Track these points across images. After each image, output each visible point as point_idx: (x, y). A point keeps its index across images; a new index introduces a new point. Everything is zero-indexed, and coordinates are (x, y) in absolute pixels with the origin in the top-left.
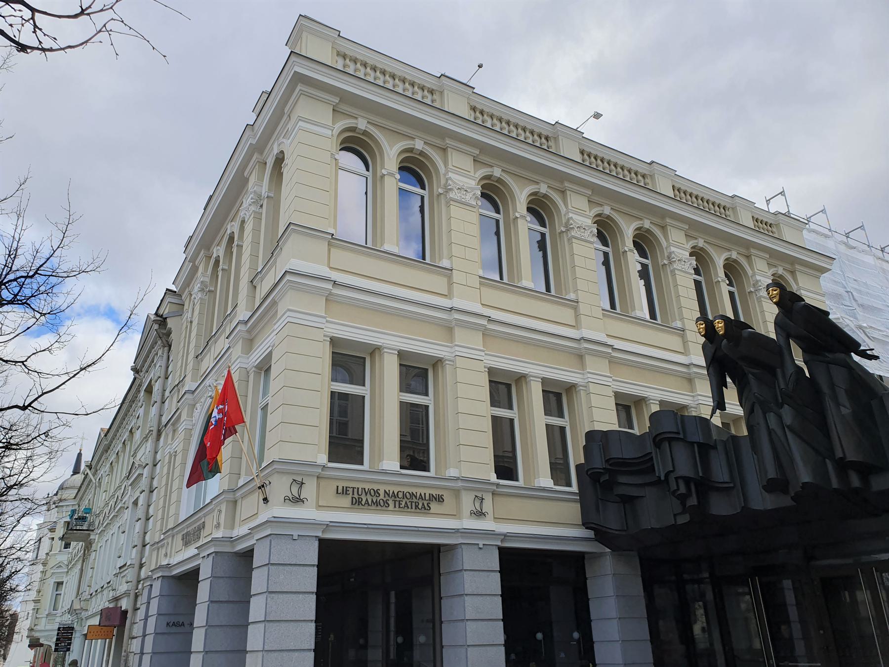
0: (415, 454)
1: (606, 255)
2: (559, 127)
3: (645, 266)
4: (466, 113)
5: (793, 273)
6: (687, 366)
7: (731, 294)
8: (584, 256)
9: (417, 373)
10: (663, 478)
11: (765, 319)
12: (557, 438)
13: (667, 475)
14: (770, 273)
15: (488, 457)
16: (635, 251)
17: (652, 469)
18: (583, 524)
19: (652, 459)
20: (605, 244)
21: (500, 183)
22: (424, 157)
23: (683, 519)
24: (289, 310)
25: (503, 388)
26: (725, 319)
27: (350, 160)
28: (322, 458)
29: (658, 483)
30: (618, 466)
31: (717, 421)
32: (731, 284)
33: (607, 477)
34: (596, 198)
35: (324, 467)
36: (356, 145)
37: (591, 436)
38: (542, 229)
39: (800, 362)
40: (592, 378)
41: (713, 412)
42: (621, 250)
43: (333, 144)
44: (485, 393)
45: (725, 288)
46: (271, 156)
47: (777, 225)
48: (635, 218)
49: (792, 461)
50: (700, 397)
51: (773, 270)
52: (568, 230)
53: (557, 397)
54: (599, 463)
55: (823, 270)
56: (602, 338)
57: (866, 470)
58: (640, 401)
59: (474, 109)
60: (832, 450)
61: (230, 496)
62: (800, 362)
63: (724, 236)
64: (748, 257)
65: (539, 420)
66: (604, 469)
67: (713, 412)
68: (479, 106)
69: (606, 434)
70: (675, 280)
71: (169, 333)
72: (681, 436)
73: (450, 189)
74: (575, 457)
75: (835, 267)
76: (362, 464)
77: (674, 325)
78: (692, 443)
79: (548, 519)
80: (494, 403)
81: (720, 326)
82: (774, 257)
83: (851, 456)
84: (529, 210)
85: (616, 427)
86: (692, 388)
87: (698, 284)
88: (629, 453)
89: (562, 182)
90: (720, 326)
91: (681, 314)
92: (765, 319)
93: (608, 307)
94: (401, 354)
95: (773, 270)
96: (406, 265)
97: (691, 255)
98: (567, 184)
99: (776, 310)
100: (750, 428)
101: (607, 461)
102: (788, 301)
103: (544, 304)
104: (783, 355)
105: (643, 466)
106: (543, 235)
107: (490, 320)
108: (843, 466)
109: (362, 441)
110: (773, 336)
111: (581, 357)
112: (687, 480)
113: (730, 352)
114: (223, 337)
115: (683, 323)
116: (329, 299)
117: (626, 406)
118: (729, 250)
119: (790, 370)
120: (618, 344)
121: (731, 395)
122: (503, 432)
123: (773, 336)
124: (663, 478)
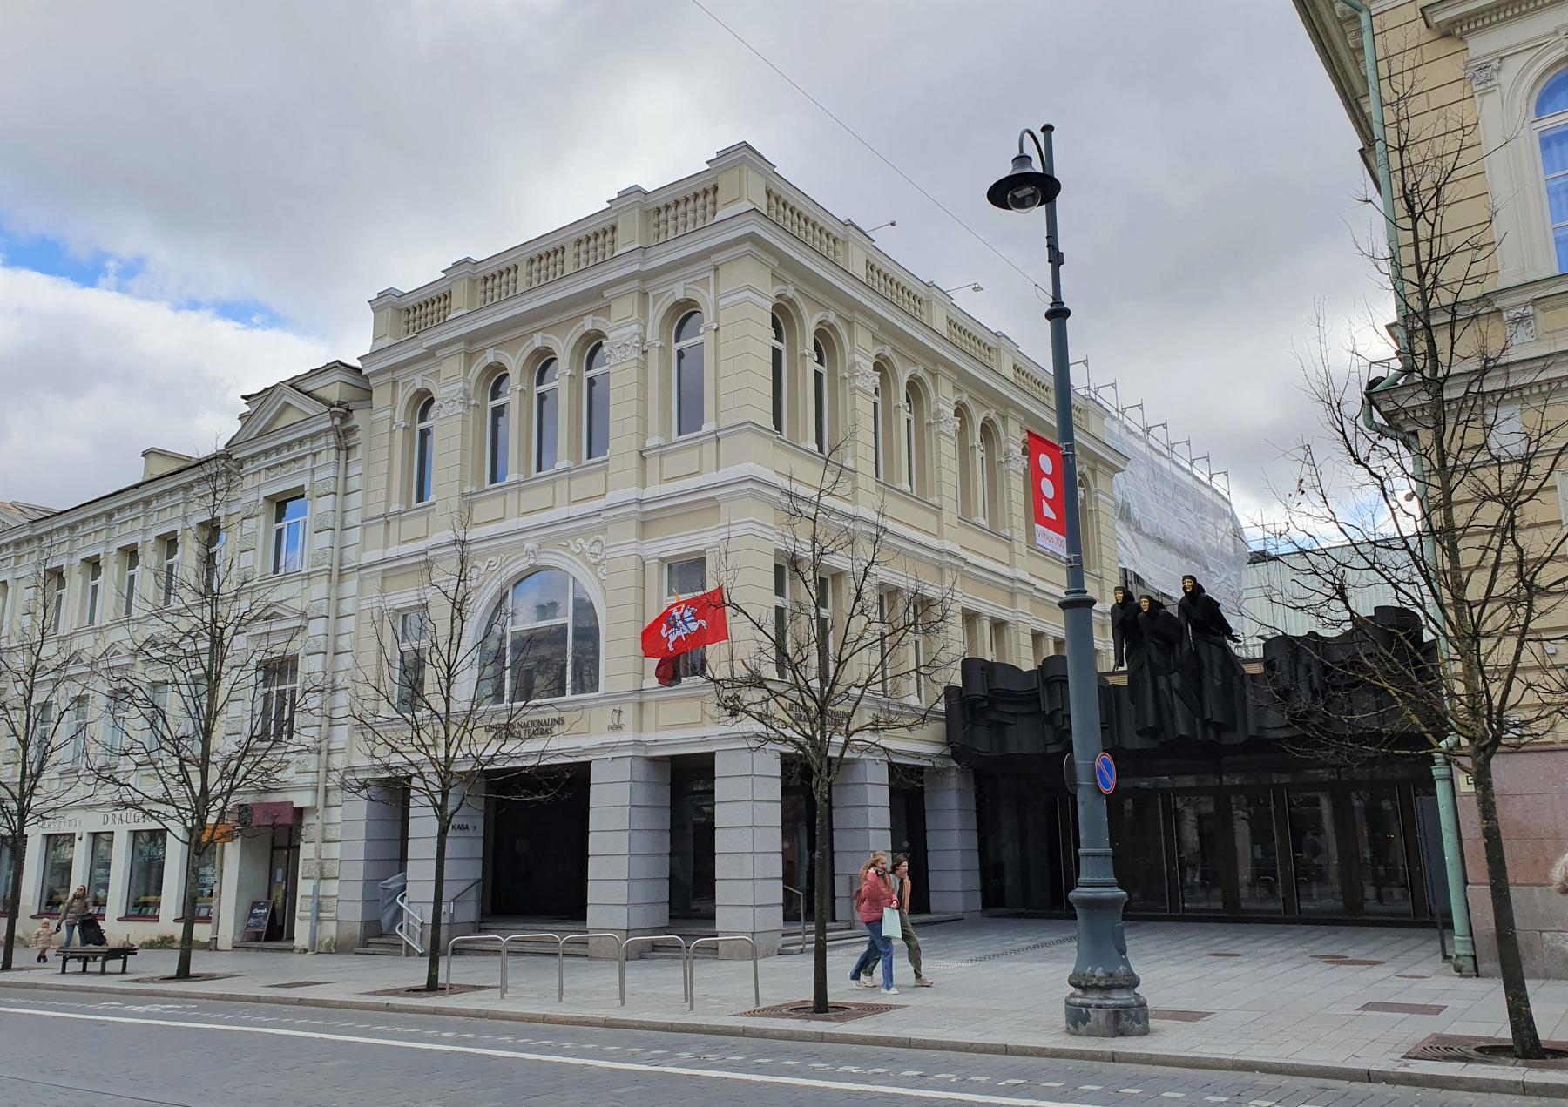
2: (935, 292)
4: (861, 271)
5: (1093, 471)
6: (1012, 580)
7: (818, 375)
8: (858, 407)
14: (772, 294)
30: (997, 697)
34: (881, 335)
40: (1022, 617)
42: (799, 352)
45: (811, 365)
47: (929, 303)
49: (1172, 715)
51: (779, 288)
52: (853, 377)
54: (979, 690)
56: (956, 549)
57: (1219, 728)
60: (1203, 712)
61: (637, 697)
64: (934, 375)
68: (878, 266)
70: (1009, 482)
71: (351, 431)
77: (975, 520)
79: (919, 744)
83: (1216, 719)
86: (1013, 605)
87: (776, 353)
89: (935, 364)
91: (1011, 521)
95: (779, 288)
98: (940, 368)
103: (1039, 562)
108: (1207, 723)
111: (1012, 594)
115: (856, 463)
118: (915, 364)
120: (1040, 584)
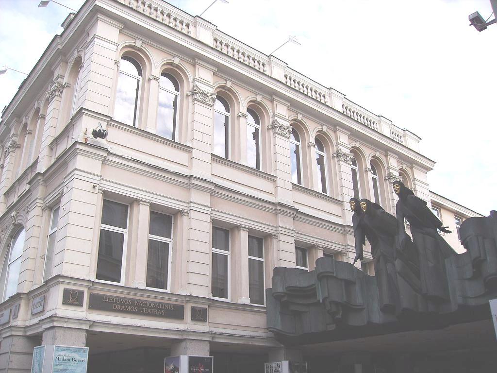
0: (157, 272)
1: (297, 146)
3: (321, 157)
4: (212, 44)
7: (374, 180)
9: (163, 219)
10: (321, 301)
11: (390, 203)
12: (256, 269)
13: (324, 300)
15: (207, 281)
16: (316, 146)
17: (315, 295)
18: (268, 329)
19: (315, 288)
20: (297, 140)
21: (229, 92)
22: (178, 69)
23: (332, 327)
24: (76, 169)
25: (222, 233)
26: (368, 202)
27: (128, 67)
28: (93, 278)
29: (318, 304)
31: (358, 265)
32: (374, 173)
33: (285, 299)
35: (93, 283)
36: (134, 57)
37: (278, 271)
38: (257, 126)
39: (408, 232)
41: (355, 261)
43: (118, 56)
44: (208, 237)
46: (72, 59)
48: (316, 123)
50: (349, 247)
53: (259, 241)
55: (428, 169)
58: (313, 247)
59: (216, 40)
62: (408, 232)
63: (372, 147)
65: (244, 257)
66: (284, 293)
67: (355, 261)
68: (220, 39)
69: (285, 269)
72: (335, 275)
73: (196, 93)
74: (268, 283)
75: (436, 167)
76: (119, 281)
78: (341, 280)
80: (215, 245)
81: (364, 206)
82: (401, 158)
84: (249, 110)
85: (294, 266)
87: (354, 171)
88: (303, 283)
90: (364, 206)
92: (390, 203)
93: (296, 183)
94: (152, 205)
96: (164, 143)
97: (351, 152)
99: (397, 198)
100: (377, 271)
101: (286, 288)
102: (405, 193)
104: (399, 227)
105: (308, 293)
106: (257, 130)
107: (216, 186)
109: (120, 262)
110: (395, 215)
112: (337, 304)
113: (368, 220)
114: (25, 182)
116: (104, 162)
117: (303, 250)
119: (401, 238)
121: (367, 248)
122: (219, 265)
123: (395, 215)
124: (321, 301)
